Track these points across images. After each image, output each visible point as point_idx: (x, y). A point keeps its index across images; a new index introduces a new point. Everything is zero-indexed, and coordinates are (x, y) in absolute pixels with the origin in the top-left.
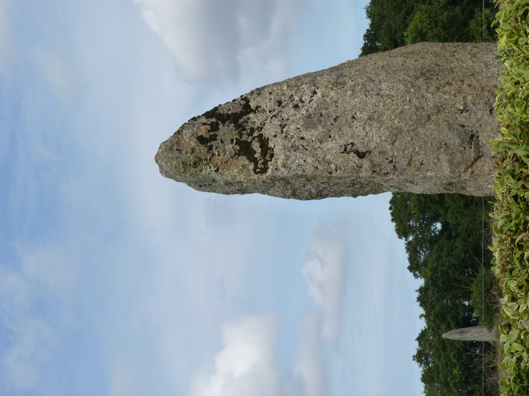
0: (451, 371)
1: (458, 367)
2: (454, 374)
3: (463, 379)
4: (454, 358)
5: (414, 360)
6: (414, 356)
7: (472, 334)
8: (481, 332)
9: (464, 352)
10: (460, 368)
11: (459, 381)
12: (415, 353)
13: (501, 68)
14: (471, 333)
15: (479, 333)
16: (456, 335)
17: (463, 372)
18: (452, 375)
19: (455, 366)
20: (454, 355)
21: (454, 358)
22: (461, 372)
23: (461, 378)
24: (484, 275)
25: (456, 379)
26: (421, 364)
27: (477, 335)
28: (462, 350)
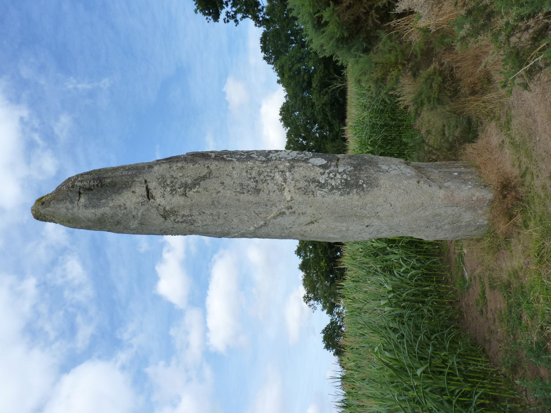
0: (319, 263)
1: (324, 261)
2: (321, 266)
3: (328, 269)
4: (322, 254)
5: (295, 253)
6: (295, 251)
7: (149, 195)
8: (194, 185)
9: (329, 249)
10: (326, 261)
11: (325, 271)
12: (296, 248)
13: (485, 86)
14: (140, 190)
15: (186, 186)
16: (72, 202)
17: (328, 264)
18: (320, 266)
19: (322, 260)
20: (322, 251)
21: (322, 254)
22: (326, 265)
23: (326, 269)
24: (403, 242)
25: (323, 269)
26: (300, 257)
27: (177, 200)
28: (327, 247)
